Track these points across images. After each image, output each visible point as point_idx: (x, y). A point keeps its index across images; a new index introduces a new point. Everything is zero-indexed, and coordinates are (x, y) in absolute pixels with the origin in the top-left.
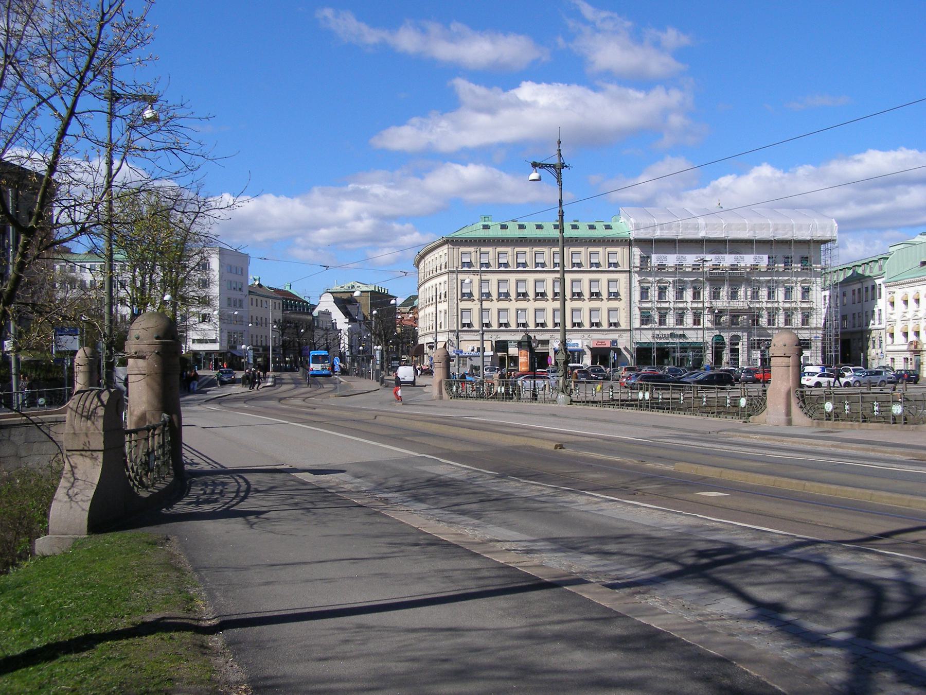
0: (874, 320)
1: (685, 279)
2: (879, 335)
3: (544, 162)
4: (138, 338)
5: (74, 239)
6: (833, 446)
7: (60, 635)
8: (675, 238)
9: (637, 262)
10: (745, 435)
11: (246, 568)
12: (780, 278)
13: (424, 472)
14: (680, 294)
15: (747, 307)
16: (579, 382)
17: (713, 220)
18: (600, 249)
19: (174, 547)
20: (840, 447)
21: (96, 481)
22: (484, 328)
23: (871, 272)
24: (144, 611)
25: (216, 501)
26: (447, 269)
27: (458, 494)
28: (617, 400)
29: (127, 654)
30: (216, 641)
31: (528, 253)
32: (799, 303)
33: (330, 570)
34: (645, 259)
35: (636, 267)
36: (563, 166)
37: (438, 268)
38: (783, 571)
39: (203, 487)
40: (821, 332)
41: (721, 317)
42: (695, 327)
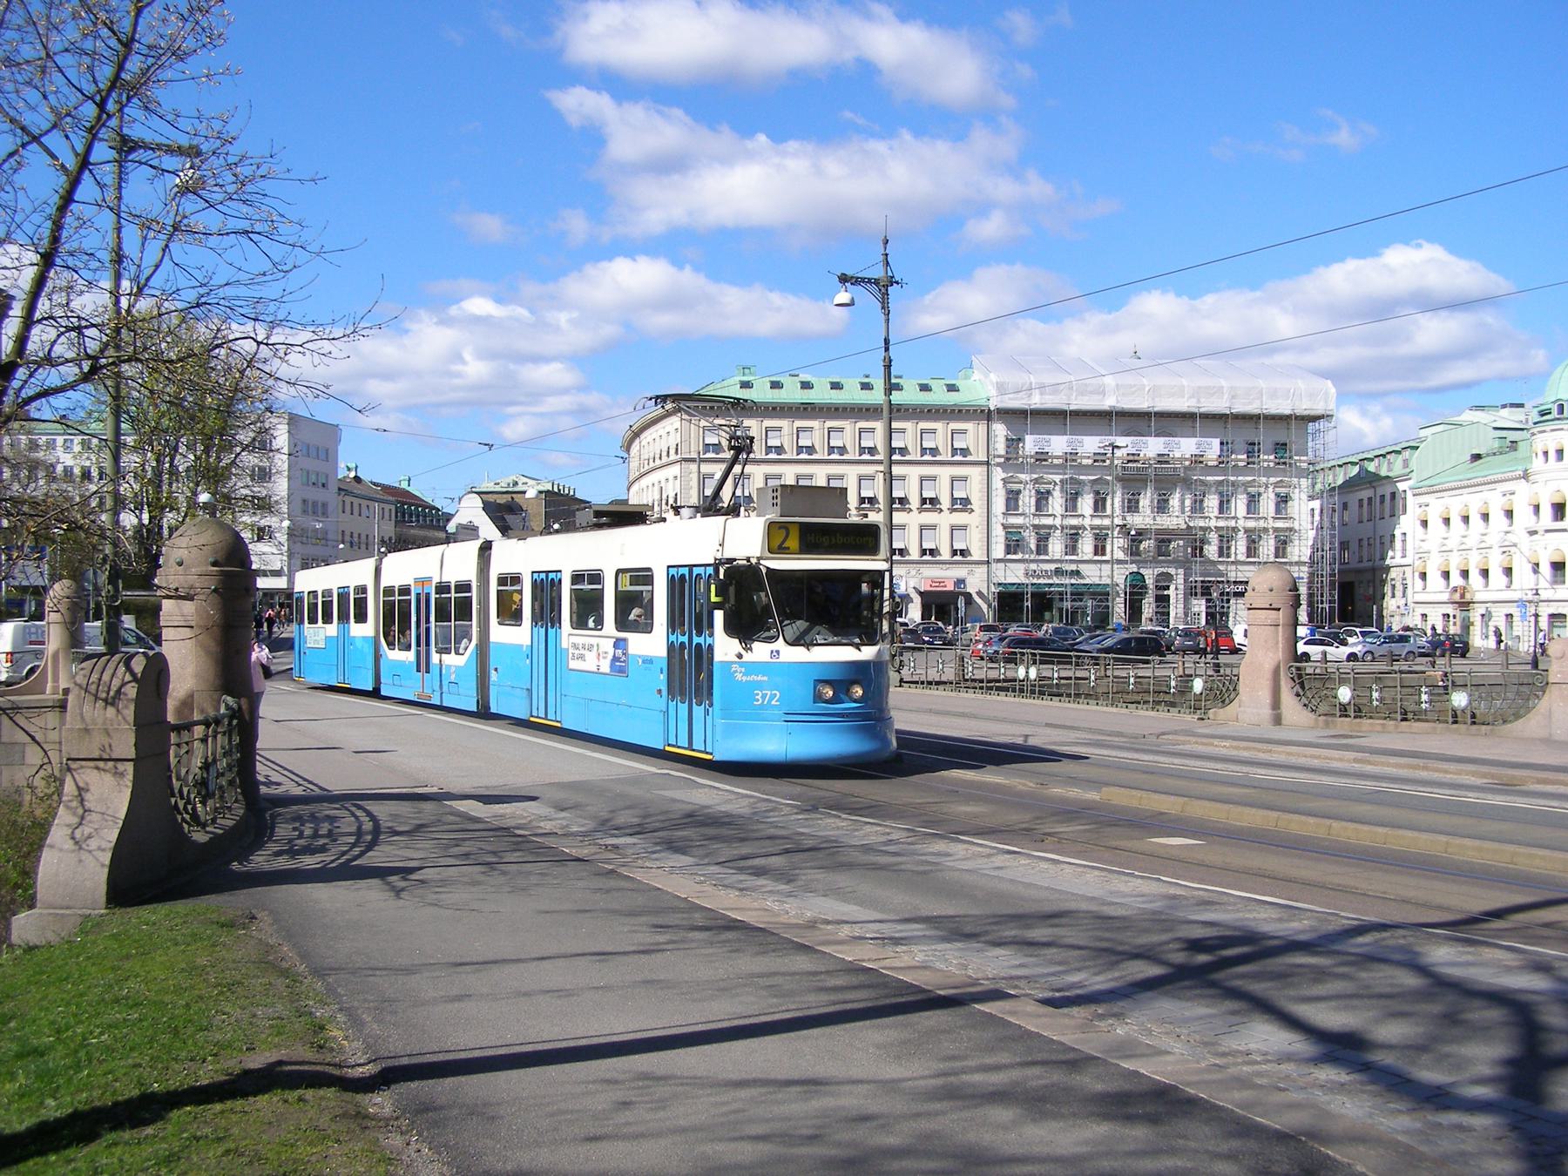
0: (1393, 550)
1: (1081, 477)
2: (1401, 575)
3: (859, 275)
4: (180, 564)
5: (79, 387)
6: (1356, 761)
7: (95, 1094)
8: (1065, 407)
9: (1000, 447)
10: (1204, 740)
11: (408, 971)
12: (1240, 478)
13: (674, 801)
14: (1072, 501)
15: (1184, 527)
16: (904, 648)
17: (1128, 379)
19: (265, 929)
20: (1370, 763)
21: (122, 814)
23: (1390, 470)
24: (241, 1049)
25: (323, 849)
26: (679, 456)
27: (743, 840)
28: (982, 681)
29: (227, 1130)
30: (380, 1103)
31: (817, 432)
32: (1271, 521)
33: (554, 975)
34: (1013, 443)
35: (999, 456)
36: (892, 281)
37: (664, 454)
38: (1343, 976)
39: (297, 825)
40: (1305, 569)
41: (1141, 542)
42: (1096, 558)
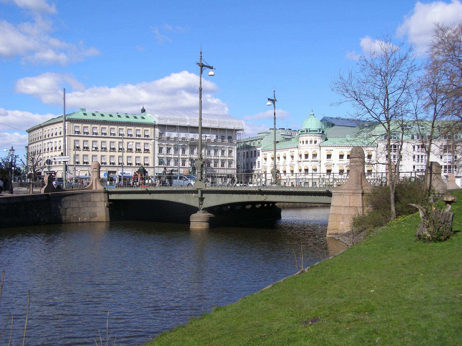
9: (157, 135)
12: (220, 146)
14: (176, 150)
18: (141, 128)
22: (76, 164)
32: (227, 157)
42: (183, 167)
